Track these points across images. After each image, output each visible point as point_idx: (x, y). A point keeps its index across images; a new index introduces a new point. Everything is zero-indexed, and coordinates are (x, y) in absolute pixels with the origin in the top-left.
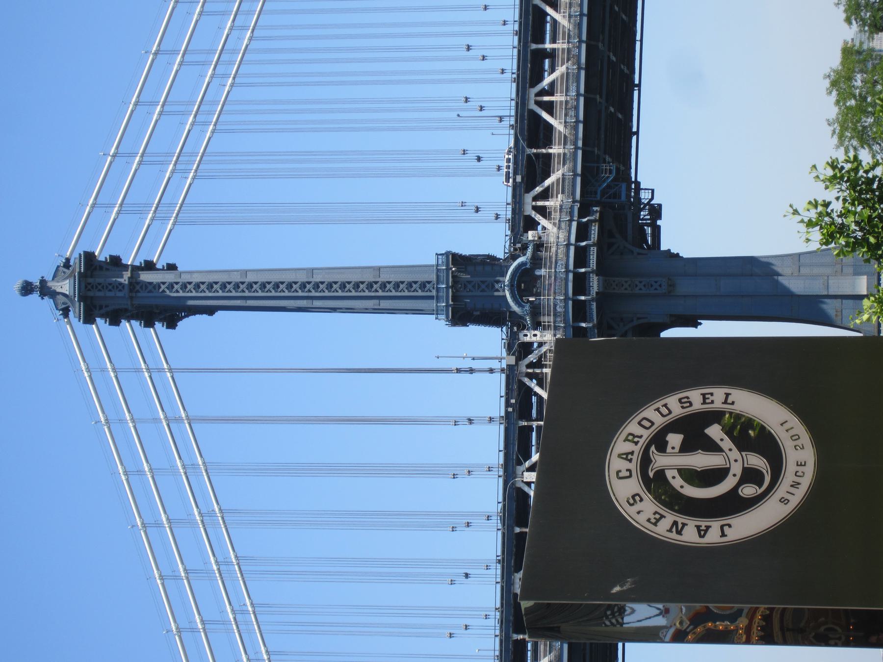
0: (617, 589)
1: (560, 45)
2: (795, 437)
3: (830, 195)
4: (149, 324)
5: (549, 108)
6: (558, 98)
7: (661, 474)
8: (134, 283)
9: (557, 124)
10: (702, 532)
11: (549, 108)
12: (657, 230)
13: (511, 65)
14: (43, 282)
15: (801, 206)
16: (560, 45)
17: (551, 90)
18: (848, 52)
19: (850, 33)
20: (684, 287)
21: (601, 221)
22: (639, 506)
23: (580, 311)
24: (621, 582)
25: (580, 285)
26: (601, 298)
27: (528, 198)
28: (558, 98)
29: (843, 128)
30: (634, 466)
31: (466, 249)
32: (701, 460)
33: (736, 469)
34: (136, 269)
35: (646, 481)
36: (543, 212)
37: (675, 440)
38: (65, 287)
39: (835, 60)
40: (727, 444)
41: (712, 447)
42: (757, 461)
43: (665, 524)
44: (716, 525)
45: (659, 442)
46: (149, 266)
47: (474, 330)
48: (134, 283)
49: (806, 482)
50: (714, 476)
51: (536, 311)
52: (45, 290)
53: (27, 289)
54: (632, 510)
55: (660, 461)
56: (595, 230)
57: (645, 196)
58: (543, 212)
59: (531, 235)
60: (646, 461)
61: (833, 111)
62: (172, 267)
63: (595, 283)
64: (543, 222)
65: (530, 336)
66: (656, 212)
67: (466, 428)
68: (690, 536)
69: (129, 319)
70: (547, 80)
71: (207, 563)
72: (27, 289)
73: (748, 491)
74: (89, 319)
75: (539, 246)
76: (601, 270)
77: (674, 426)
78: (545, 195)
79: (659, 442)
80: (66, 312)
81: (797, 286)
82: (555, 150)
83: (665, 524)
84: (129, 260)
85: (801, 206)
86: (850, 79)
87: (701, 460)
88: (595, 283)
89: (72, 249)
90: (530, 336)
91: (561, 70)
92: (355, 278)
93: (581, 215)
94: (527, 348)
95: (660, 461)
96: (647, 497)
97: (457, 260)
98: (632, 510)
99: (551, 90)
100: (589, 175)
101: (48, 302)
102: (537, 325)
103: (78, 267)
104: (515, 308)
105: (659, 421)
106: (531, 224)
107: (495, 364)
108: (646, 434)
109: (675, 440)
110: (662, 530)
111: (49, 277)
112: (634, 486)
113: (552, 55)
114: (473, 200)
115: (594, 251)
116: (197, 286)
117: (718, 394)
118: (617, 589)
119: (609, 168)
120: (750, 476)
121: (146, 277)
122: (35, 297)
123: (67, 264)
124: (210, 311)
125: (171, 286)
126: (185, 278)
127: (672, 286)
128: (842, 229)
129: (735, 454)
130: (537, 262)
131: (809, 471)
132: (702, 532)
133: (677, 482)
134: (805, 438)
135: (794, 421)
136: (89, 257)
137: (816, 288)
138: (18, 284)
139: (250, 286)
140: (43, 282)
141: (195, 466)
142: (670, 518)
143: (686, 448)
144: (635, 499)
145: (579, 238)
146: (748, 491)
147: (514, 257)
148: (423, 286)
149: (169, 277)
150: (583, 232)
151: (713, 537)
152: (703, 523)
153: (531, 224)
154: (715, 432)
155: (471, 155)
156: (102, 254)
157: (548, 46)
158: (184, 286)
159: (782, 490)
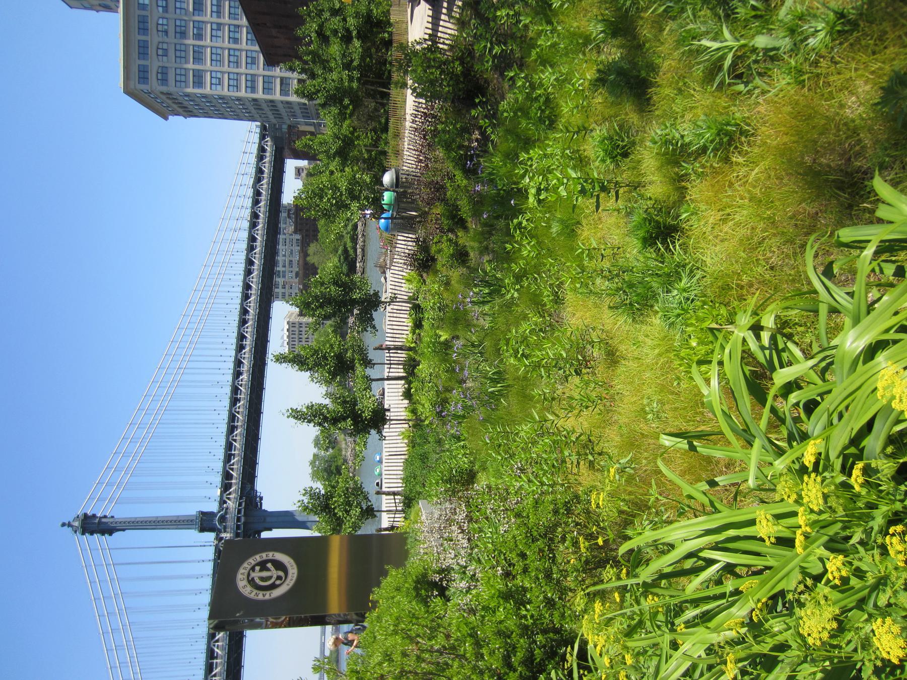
0: (238, 615)
1: (237, 452)
2: (292, 566)
3: (304, 498)
4: (103, 534)
5: (232, 469)
6: (235, 467)
7: (253, 579)
8: (100, 522)
9: (234, 474)
10: (264, 595)
11: (232, 469)
12: (261, 504)
13: (234, 347)
14: (69, 522)
15: (296, 503)
16: (237, 452)
17: (233, 465)
18: (315, 455)
19: (315, 450)
20: (268, 519)
21: (246, 502)
22: (246, 589)
23: (238, 527)
24: (239, 613)
25: (239, 519)
26: (245, 523)
27: (225, 495)
28: (235, 467)
29: (313, 475)
30: (245, 577)
31: (205, 510)
32: (265, 574)
33: (275, 576)
34: (101, 518)
35: (249, 582)
36: (229, 499)
37: (257, 568)
38: (76, 524)
39: (311, 458)
40: (272, 568)
41: (268, 570)
42: (281, 573)
43: (253, 594)
44: (268, 593)
45: (253, 569)
46: (105, 517)
47: (206, 533)
48: (100, 522)
49: (294, 579)
50: (270, 578)
51: (225, 528)
52: (69, 525)
53: (63, 525)
54: (244, 590)
55: (253, 575)
56: (243, 511)
57: (258, 494)
58: (229, 499)
59: (225, 505)
60: (249, 575)
61: (310, 471)
62: (113, 517)
63: (243, 519)
64: (228, 501)
65: (223, 535)
66: (261, 498)
67: (202, 563)
68: (260, 597)
69: (96, 533)
70: (232, 462)
71: (115, 610)
72: (63, 525)
73: (278, 582)
74: (83, 534)
75: (227, 509)
76: (245, 515)
77: (258, 564)
78: (230, 494)
79: (253, 569)
80: (76, 532)
81: (300, 518)
82: (233, 481)
83: (253, 594)
84: (99, 515)
85: (296, 502)
86: (315, 462)
87: (265, 574)
88: (243, 519)
89: (80, 512)
90: (223, 535)
91: (236, 459)
92: (170, 519)
93: (240, 499)
94: (222, 539)
95: (253, 575)
96: (249, 586)
97: (203, 513)
98: (244, 590)
99: (233, 465)
100: (243, 488)
101: (70, 529)
102: (225, 531)
103: (82, 517)
104: (219, 527)
105: (253, 563)
106: (225, 502)
107: (212, 544)
108: (249, 567)
109: (257, 568)
110: (252, 596)
111: (71, 521)
112: (245, 582)
113: (234, 455)
114: (208, 496)
115: (243, 510)
116: (120, 523)
117: (271, 554)
118: (238, 615)
119: (248, 486)
120: (279, 578)
121: (104, 520)
122: (66, 527)
123: (78, 517)
124: (124, 530)
125: (112, 523)
126: (117, 520)
127: (265, 519)
128: (307, 507)
129: (275, 572)
130: (226, 513)
131: (295, 575)
132: (264, 595)
133: (257, 581)
134: (295, 566)
135: (292, 561)
136: (86, 515)
137: (305, 519)
138: (60, 523)
139: (137, 522)
140: (69, 522)
141: (114, 579)
142: (255, 591)
143: (261, 570)
144: (245, 587)
145: (239, 506)
146: (278, 582)
147: (219, 512)
148: (191, 521)
149: (111, 520)
150: (240, 505)
151: (267, 597)
152: (264, 592)
153: (225, 502)
154: (269, 565)
155: (211, 468)
156: (89, 513)
157: (236, 424)
158: (116, 523)
159: (288, 581)
